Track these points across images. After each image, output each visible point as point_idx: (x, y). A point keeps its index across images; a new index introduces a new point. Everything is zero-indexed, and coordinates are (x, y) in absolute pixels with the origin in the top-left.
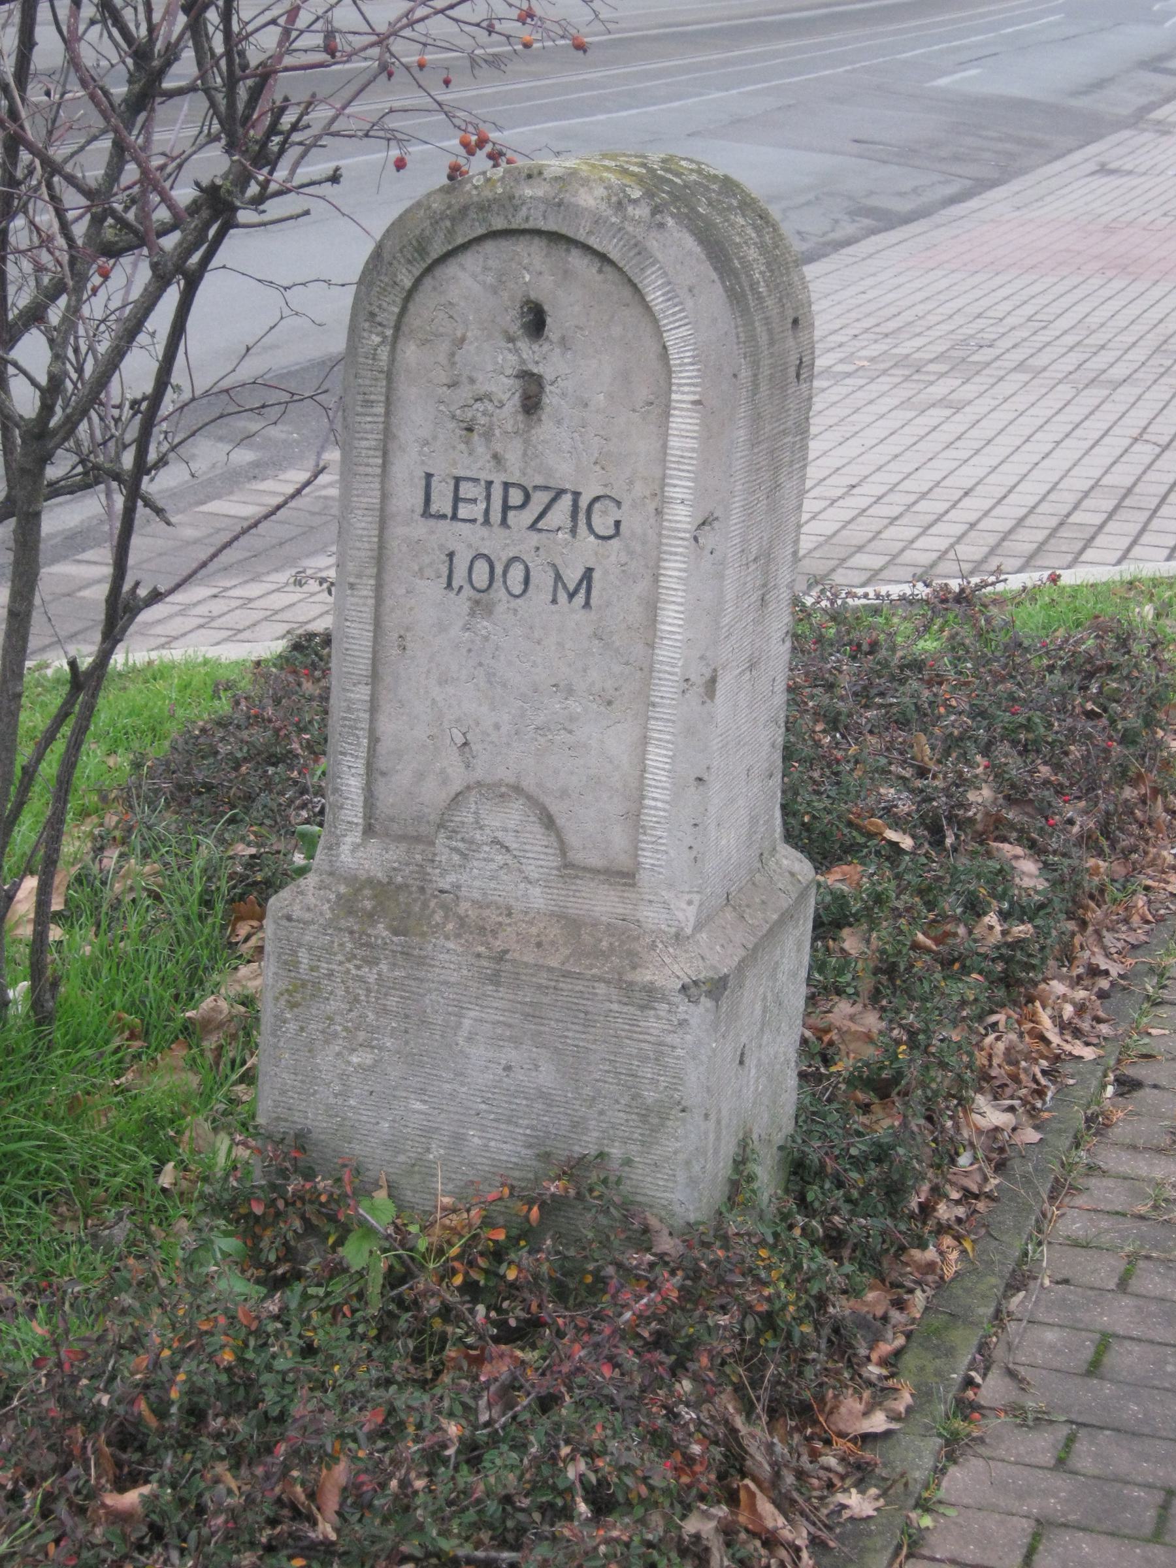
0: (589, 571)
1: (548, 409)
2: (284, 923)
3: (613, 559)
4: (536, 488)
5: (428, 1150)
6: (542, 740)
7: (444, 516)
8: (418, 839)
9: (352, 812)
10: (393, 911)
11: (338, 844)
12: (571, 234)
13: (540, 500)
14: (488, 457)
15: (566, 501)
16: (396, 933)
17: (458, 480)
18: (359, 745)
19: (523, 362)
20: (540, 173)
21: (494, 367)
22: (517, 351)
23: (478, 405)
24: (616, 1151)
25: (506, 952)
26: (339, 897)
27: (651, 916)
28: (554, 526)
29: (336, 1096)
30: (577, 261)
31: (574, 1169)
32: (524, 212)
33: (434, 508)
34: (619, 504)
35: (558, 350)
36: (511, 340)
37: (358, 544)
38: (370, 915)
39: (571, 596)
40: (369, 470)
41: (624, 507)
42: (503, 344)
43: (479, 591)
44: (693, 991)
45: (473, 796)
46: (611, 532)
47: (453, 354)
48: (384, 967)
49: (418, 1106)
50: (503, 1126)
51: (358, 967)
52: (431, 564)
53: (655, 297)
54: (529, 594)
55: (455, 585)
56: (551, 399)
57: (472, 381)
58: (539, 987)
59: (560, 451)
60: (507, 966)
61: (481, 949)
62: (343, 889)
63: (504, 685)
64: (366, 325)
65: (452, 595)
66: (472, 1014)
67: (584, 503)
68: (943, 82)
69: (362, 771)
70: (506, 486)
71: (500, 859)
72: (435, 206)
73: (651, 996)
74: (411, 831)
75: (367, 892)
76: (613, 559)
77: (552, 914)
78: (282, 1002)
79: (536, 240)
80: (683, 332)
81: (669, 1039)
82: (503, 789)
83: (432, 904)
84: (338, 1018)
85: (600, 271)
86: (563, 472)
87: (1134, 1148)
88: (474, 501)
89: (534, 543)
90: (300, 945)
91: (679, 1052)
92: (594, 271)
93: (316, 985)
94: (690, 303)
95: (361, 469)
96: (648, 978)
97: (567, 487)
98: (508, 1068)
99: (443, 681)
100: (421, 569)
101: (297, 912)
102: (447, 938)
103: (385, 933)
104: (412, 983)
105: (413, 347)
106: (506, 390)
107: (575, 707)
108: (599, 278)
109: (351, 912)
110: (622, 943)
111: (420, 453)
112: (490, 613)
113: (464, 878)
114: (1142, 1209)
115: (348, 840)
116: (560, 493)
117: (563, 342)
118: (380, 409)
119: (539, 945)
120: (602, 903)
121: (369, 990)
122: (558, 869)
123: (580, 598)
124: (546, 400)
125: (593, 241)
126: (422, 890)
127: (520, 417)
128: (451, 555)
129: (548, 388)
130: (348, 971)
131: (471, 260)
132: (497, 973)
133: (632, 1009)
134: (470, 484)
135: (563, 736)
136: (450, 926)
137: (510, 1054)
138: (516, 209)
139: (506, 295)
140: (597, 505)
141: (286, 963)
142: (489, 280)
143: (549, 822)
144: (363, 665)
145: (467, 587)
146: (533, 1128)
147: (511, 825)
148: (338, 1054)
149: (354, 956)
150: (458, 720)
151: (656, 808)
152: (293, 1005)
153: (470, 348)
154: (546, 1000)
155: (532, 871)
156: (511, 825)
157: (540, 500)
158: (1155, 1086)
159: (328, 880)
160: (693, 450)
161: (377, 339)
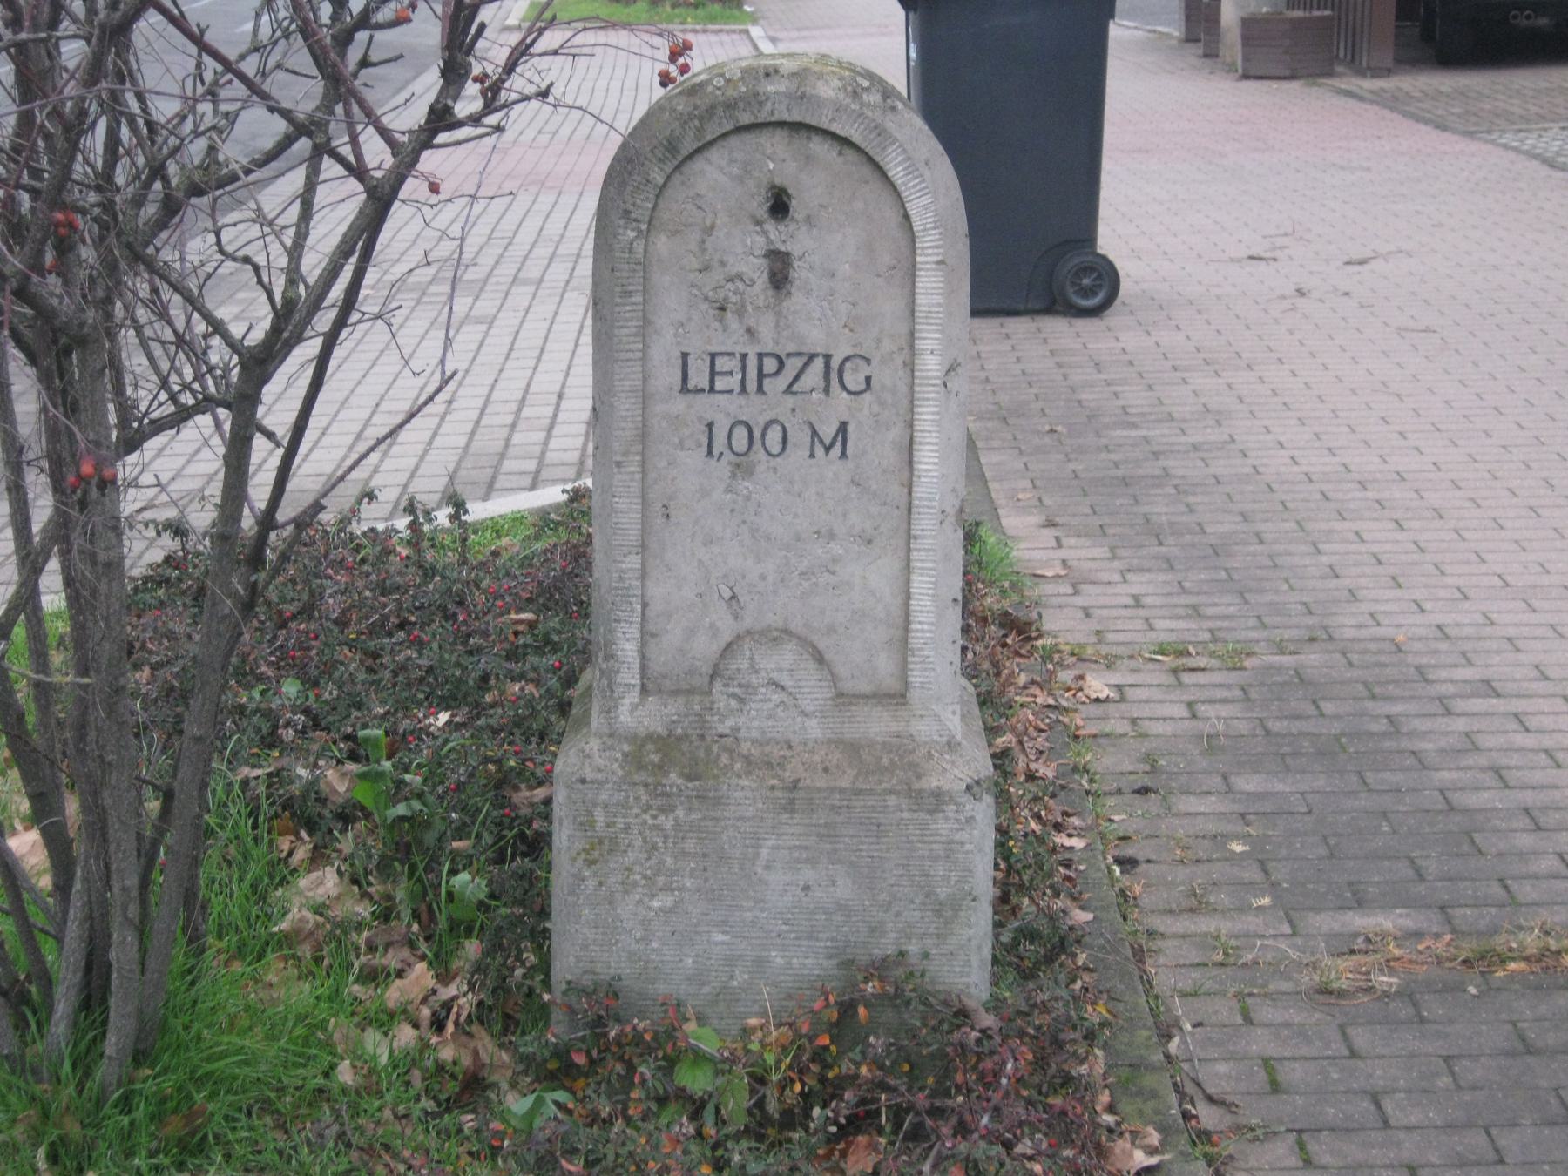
1: (797, 282)
2: (580, 786)
3: (866, 411)
4: (789, 355)
5: (732, 977)
6: (806, 584)
7: (703, 390)
8: (691, 691)
9: (630, 675)
10: (679, 761)
11: (616, 707)
12: (814, 123)
13: (793, 365)
14: (742, 331)
15: (819, 363)
16: (689, 778)
17: (713, 356)
18: (632, 611)
19: (770, 242)
20: (776, 71)
21: (744, 250)
23: (729, 285)
24: (913, 948)
25: (798, 780)
26: (625, 755)
27: (924, 730)
28: (808, 388)
29: (638, 942)
30: (818, 146)
31: (879, 968)
32: (769, 106)
33: (691, 384)
35: (804, 229)
36: (759, 223)
37: (623, 425)
38: (660, 767)
39: (827, 449)
40: (631, 355)
41: (874, 363)
42: (751, 227)
43: (737, 454)
44: (976, 789)
46: (863, 386)
47: (703, 242)
48: (680, 812)
49: (720, 937)
50: (805, 943)
52: (692, 435)
53: (897, 173)
54: (788, 451)
55: (716, 452)
56: (799, 273)
57: (723, 264)
58: (833, 807)
59: (812, 320)
60: (800, 794)
61: (775, 782)
62: (626, 748)
64: (622, 222)
65: (713, 462)
66: (770, 843)
67: (835, 363)
69: (637, 635)
70: (760, 356)
72: (680, 108)
73: (939, 799)
75: (650, 747)
76: (866, 411)
77: (830, 741)
78: (580, 861)
79: (778, 131)
80: (925, 201)
81: (958, 837)
82: (775, 634)
83: (715, 748)
84: (637, 868)
85: (840, 154)
86: (815, 339)
87: (1171, 912)
88: (731, 373)
89: (791, 406)
90: (595, 805)
91: (968, 847)
92: (834, 154)
93: (614, 841)
94: (927, 174)
95: (623, 355)
96: (935, 784)
97: (819, 350)
98: (806, 888)
99: (708, 542)
100: (681, 442)
101: (589, 776)
102: (739, 776)
103: (680, 781)
104: (709, 823)
105: (663, 238)
106: (756, 270)
107: (837, 549)
108: (841, 159)
109: (640, 767)
110: (901, 757)
111: (676, 335)
112: (752, 474)
114: (1220, 957)
115: (627, 701)
116: (812, 357)
117: (809, 220)
118: (638, 298)
119: (826, 770)
120: (877, 724)
121: (666, 837)
122: (832, 699)
124: (793, 274)
125: (836, 128)
126: (702, 737)
127: (770, 292)
128: (710, 426)
130: (645, 822)
131: (714, 154)
132: (792, 802)
133: (922, 815)
134: (726, 358)
136: (738, 766)
137: (808, 875)
138: (761, 104)
139: (751, 183)
140: (848, 365)
141: (581, 824)
143: (819, 658)
144: (633, 536)
145: (727, 452)
146: (833, 939)
147: (786, 665)
148: (639, 902)
149: (650, 807)
150: (725, 576)
151: (922, 631)
152: (591, 863)
153: (719, 233)
154: (839, 819)
155: (807, 704)
156: (786, 665)
157: (793, 365)
158: (1149, 861)
160: (939, 305)
161: (632, 234)
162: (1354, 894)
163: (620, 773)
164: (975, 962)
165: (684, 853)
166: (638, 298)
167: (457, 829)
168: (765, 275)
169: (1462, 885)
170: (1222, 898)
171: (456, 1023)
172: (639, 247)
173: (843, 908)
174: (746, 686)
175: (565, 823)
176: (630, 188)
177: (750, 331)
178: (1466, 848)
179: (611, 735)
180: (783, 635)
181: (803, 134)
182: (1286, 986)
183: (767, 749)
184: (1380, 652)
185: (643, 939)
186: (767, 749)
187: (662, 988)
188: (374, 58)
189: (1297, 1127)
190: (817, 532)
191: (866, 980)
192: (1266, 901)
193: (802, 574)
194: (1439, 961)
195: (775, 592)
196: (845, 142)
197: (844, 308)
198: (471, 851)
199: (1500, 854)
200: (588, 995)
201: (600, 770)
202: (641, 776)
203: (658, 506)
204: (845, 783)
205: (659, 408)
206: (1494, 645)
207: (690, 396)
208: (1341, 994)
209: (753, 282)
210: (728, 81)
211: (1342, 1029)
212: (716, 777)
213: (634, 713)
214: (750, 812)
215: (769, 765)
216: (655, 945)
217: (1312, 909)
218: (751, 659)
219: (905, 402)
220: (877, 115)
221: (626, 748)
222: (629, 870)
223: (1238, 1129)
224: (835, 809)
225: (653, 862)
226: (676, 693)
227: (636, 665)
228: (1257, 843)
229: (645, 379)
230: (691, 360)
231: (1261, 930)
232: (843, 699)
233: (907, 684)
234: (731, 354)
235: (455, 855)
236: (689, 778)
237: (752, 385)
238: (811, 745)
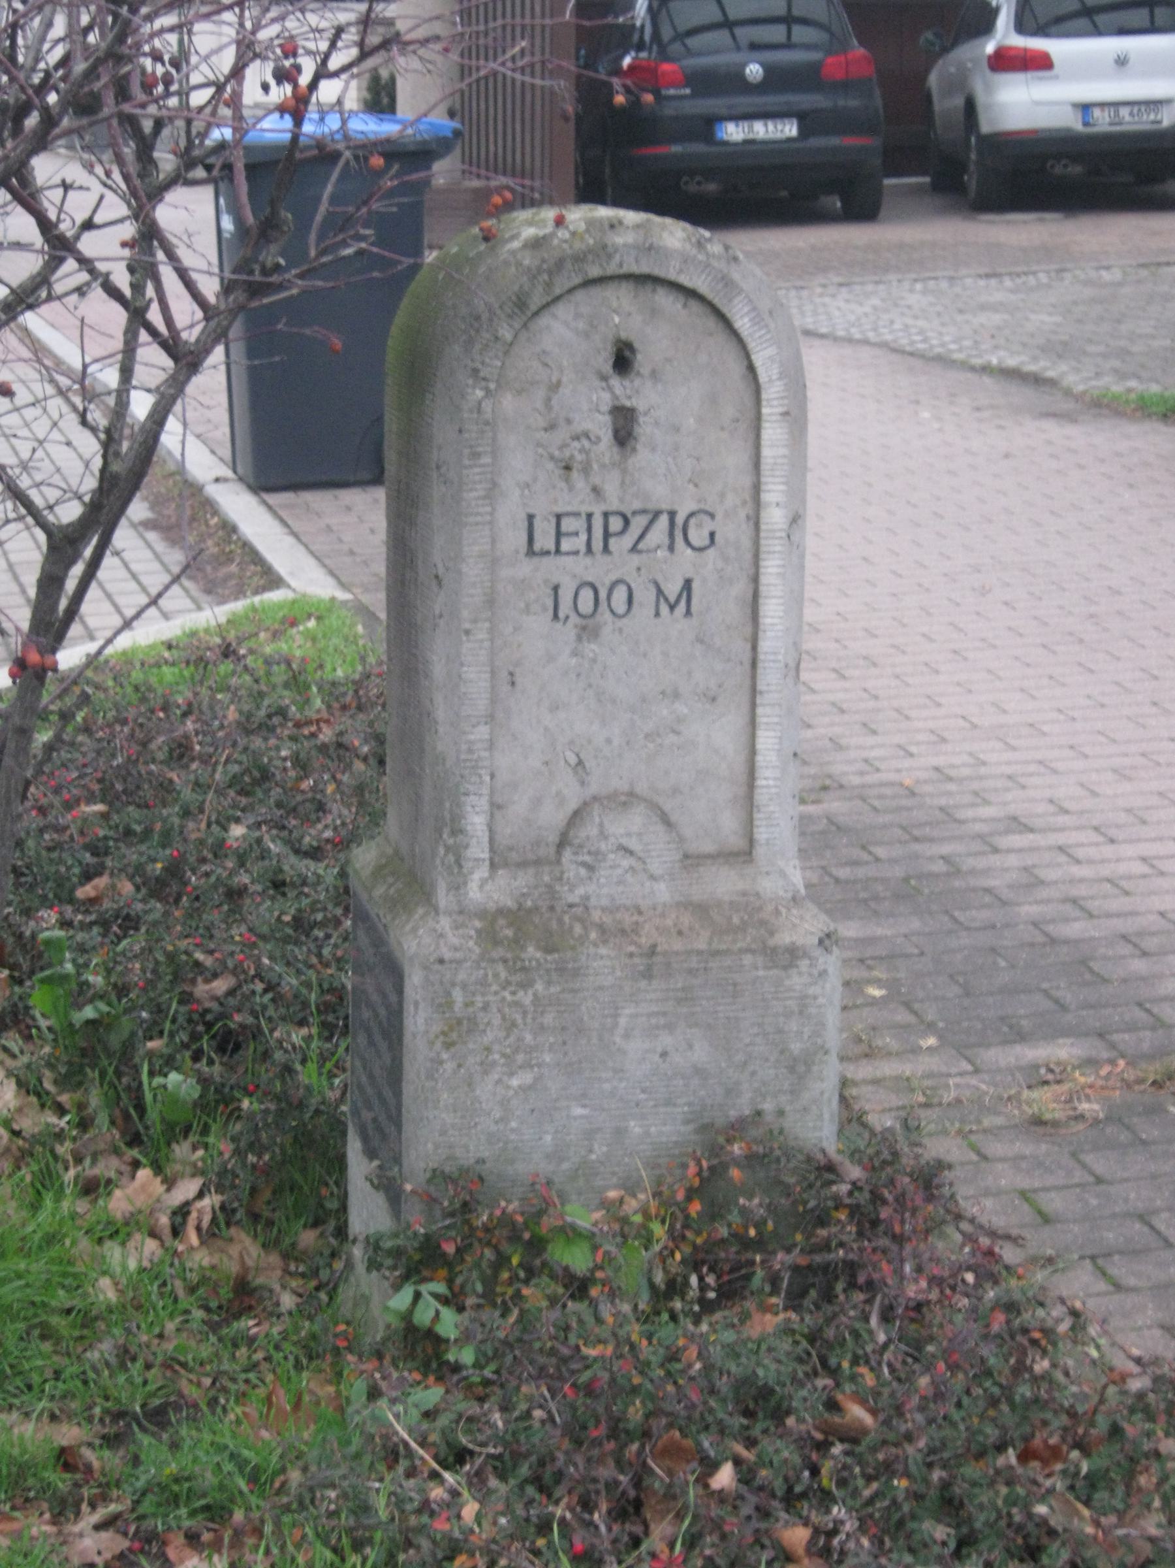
1: (643, 439)
2: (437, 967)
3: (710, 566)
4: (634, 513)
5: (591, 1151)
7: (548, 553)
8: (538, 862)
9: (478, 850)
10: (531, 935)
11: (465, 883)
17: (559, 517)
21: (589, 405)
22: (610, 389)
23: (576, 444)
24: (768, 1106)
26: (479, 932)
27: (769, 886)
28: (653, 545)
30: (665, 300)
31: (736, 1129)
32: (617, 258)
33: (537, 547)
34: (712, 516)
35: (649, 384)
36: (604, 378)
38: (516, 941)
39: (672, 608)
41: (719, 517)
42: (597, 383)
45: (596, 809)
46: (707, 542)
47: (549, 399)
48: (539, 986)
49: (578, 1111)
51: (514, 993)
53: (743, 324)
55: (561, 615)
56: (645, 428)
57: (569, 421)
58: (690, 971)
59: (656, 476)
60: (658, 959)
61: (632, 948)
62: (478, 924)
63: (614, 701)
65: (559, 625)
67: (680, 520)
68: (676, 149)
70: (606, 515)
71: (626, 862)
72: (527, 262)
73: (794, 954)
74: (531, 856)
75: (502, 922)
76: (710, 566)
77: (678, 904)
78: (438, 1045)
79: (624, 285)
81: (811, 991)
83: (566, 919)
84: (496, 1047)
86: (659, 494)
90: (453, 985)
91: (821, 1000)
93: (473, 1020)
95: (471, 519)
97: (664, 507)
98: (664, 1054)
99: (554, 708)
100: (528, 606)
101: (447, 955)
103: (538, 955)
105: (509, 396)
106: (602, 426)
107: (681, 709)
109: (496, 942)
111: (522, 496)
113: (591, 888)
116: (657, 514)
117: (654, 375)
119: (680, 933)
120: (723, 884)
121: (525, 1013)
124: (638, 430)
125: (684, 280)
126: (552, 908)
127: (615, 449)
128: (556, 589)
129: (641, 419)
131: (562, 310)
132: (649, 968)
135: (672, 738)
136: (593, 935)
137: (666, 1040)
138: (610, 257)
140: (693, 521)
142: (581, 325)
144: (482, 705)
146: (689, 1104)
149: (508, 983)
150: (571, 742)
152: (448, 1046)
153: (566, 391)
155: (655, 867)
156: (635, 829)
157: (638, 523)
159: (460, 919)
162: (1011, 1027)
163: (477, 950)
164: (826, 1116)
165: (542, 1028)
166: (486, 460)
167: (149, 1029)
168: (610, 433)
169: (1107, 1012)
170: (888, 1041)
171: (198, 1229)
172: (487, 406)
174: (596, 853)
175: (422, 1005)
176: (478, 347)
177: (596, 490)
178: (1088, 976)
180: (626, 800)
181: (649, 287)
182: (999, 1121)
183: (618, 916)
184: (894, 797)
185: (502, 1119)
186: (618, 916)
187: (522, 1169)
188: (98, 219)
189: (1088, 1252)
190: (663, 693)
191: (729, 1141)
192: (932, 1041)
193: (647, 736)
194: (1128, 1085)
195: (620, 756)
196: (691, 294)
198: (166, 1051)
199: (1125, 981)
200: (454, 1182)
201: (456, 949)
202: (500, 952)
203: (504, 674)
204: (702, 945)
205: (505, 572)
206: (999, 784)
207: (536, 560)
208: (1055, 1124)
209: (599, 439)
210: (574, 234)
211: (1073, 1155)
212: (573, 948)
213: (484, 888)
214: (609, 981)
215: (623, 932)
216: (513, 1124)
217: (980, 1045)
218: (601, 825)
219: (748, 556)
220: (720, 265)
221: (478, 924)
222: (488, 1049)
223: (1033, 1260)
225: (512, 1039)
226: (523, 865)
227: (486, 839)
228: (892, 986)
229: (493, 541)
230: (537, 523)
231: (944, 1069)
232: (691, 861)
233: (751, 841)
234: (577, 514)
235: (151, 1054)
236: (548, 950)
237: (598, 544)
238: (660, 909)
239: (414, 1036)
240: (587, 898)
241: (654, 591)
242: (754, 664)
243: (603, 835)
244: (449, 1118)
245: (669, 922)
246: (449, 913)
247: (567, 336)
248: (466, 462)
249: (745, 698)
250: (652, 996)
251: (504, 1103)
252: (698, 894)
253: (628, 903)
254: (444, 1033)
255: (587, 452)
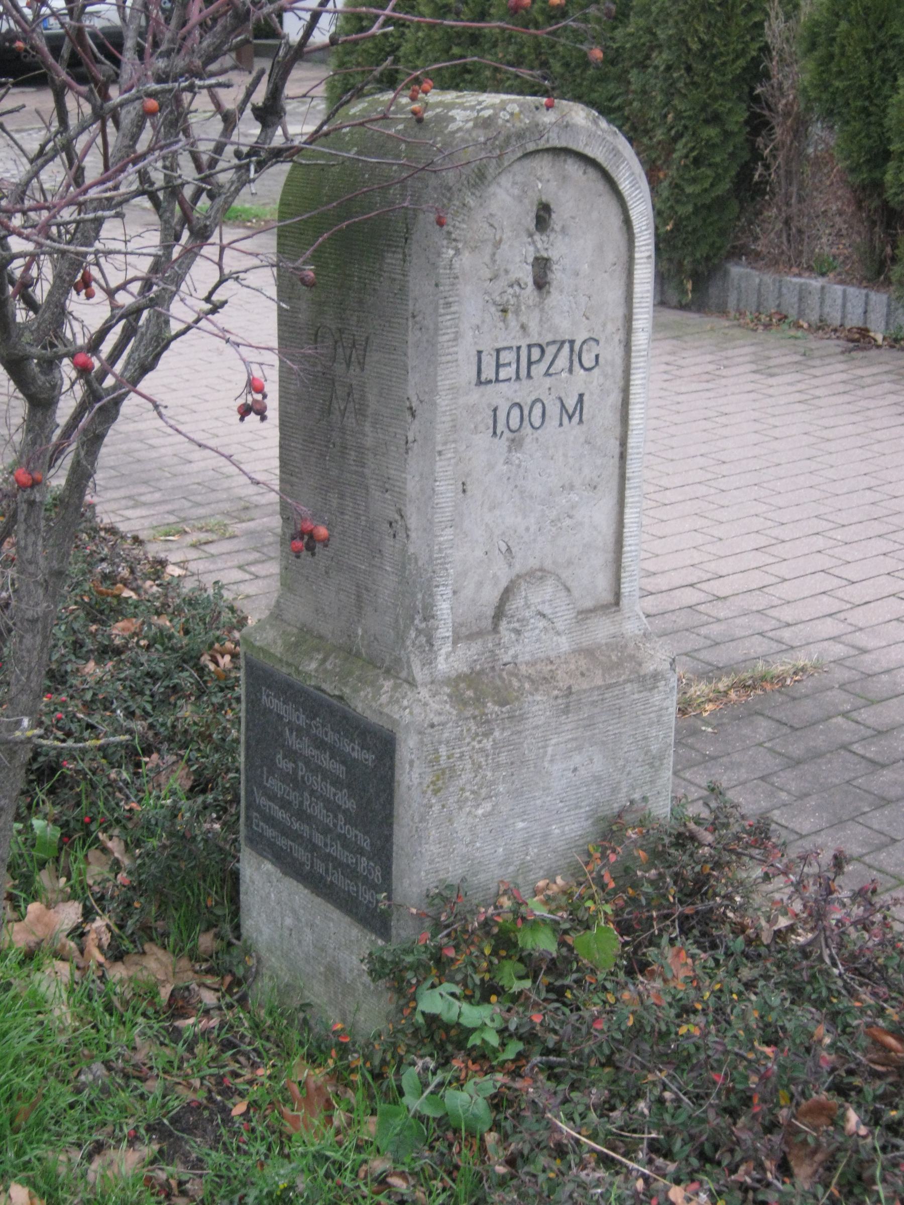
0: (581, 396)
1: (555, 283)
2: (429, 730)
4: (548, 344)
7: (490, 382)
8: (480, 634)
10: (485, 692)
17: (498, 351)
19: (537, 250)
23: (510, 291)
24: (637, 796)
26: (450, 696)
30: (573, 168)
33: (483, 377)
36: (531, 235)
39: (570, 418)
48: (497, 733)
49: (521, 825)
51: (480, 742)
55: (498, 432)
56: (557, 276)
57: (507, 272)
59: (563, 315)
60: (574, 697)
61: (556, 692)
63: (531, 497)
64: (445, 242)
65: (496, 440)
66: (553, 742)
70: (530, 347)
71: (542, 624)
74: (475, 629)
75: (462, 685)
77: (574, 651)
84: (468, 787)
90: (440, 743)
92: (581, 172)
93: (452, 769)
95: (444, 359)
98: (575, 770)
99: (492, 508)
101: (436, 720)
106: (526, 274)
108: (584, 178)
109: (465, 704)
111: (474, 337)
113: (518, 648)
115: (443, 651)
119: (583, 674)
120: (602, 630)
123: (576, 418)
124: (551, 276)
126: (493, 668)
128: (495, 410)
129: (554, 267)
135: (568, 522)
137: (577, 759)
139: (526, 201)
142: (516, 192)
145: (506, 431)
149: (477, 735)
152: (436, 792)
153: (504, 247)
154: (597, 710)
156: (548, 598)
157: (551, 351)
159: (434, 688)
165: (499, 765)
171: (100, 947)
173: (597, 779)
175: (417, 763)
177: (523, 327)
179: (432, 682)
180: (538, 575)
183: (538, 667)
195: (535, 540)
197: (583, 300)
204: (600, 682)
207: (482, 387)
212: (517, 698)
213: (450, 660)
219: (619, 372)
221: (447, 690)
222: (463, 789)
224: (594, 703)
236: (502, 704)
239: (409, 788)
240: (515, 656)
241: (559, 405)
242: (623, 456)
243: (528, 606)
244: (435, 849)
245: (573, 667)
246: (425, 685)
247: (505, 201)
248: (442, 311)
249: (614, 483)
250: (569, 727)
251: (472, 829)
252: (586, 641)
253: (542, 655)
254: (433, 783)
255: (517, 296)
